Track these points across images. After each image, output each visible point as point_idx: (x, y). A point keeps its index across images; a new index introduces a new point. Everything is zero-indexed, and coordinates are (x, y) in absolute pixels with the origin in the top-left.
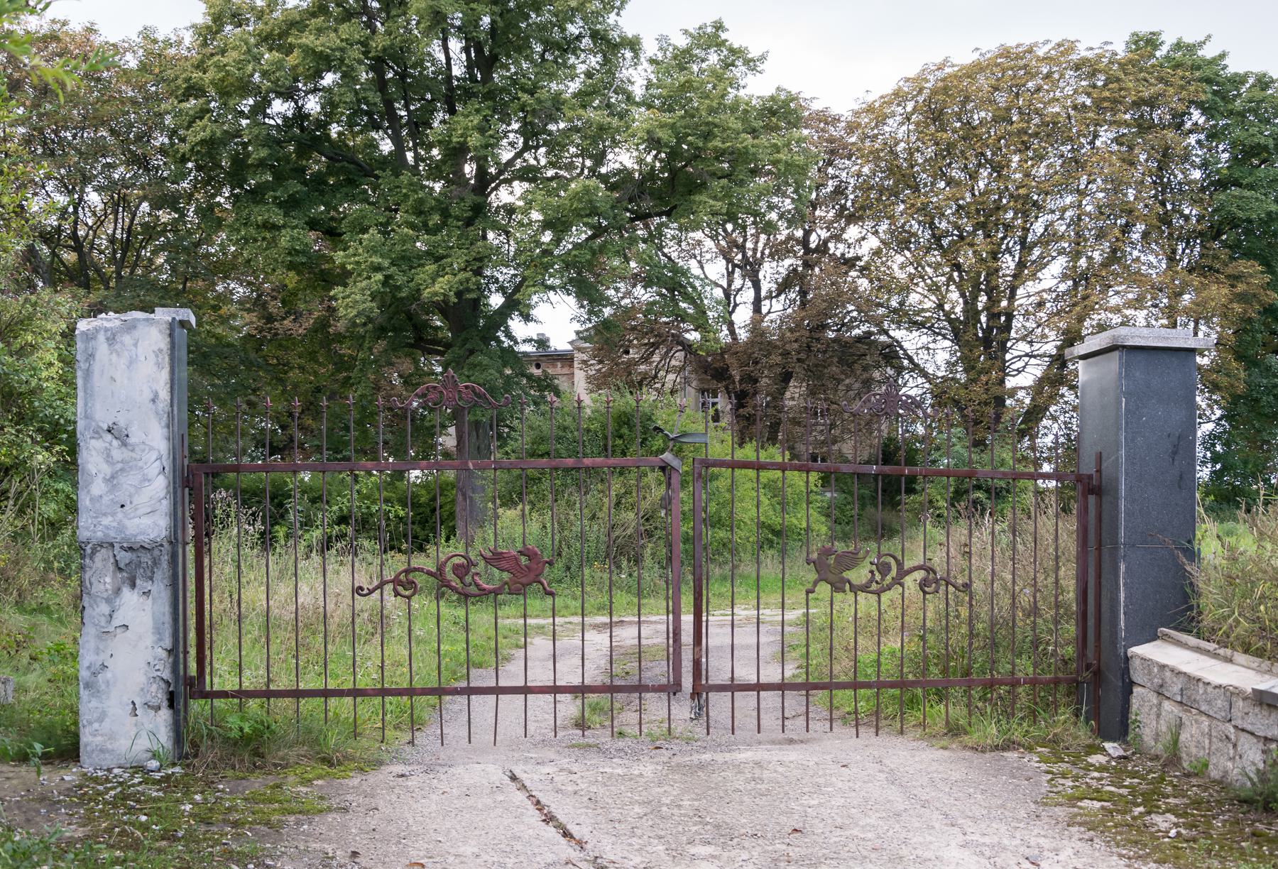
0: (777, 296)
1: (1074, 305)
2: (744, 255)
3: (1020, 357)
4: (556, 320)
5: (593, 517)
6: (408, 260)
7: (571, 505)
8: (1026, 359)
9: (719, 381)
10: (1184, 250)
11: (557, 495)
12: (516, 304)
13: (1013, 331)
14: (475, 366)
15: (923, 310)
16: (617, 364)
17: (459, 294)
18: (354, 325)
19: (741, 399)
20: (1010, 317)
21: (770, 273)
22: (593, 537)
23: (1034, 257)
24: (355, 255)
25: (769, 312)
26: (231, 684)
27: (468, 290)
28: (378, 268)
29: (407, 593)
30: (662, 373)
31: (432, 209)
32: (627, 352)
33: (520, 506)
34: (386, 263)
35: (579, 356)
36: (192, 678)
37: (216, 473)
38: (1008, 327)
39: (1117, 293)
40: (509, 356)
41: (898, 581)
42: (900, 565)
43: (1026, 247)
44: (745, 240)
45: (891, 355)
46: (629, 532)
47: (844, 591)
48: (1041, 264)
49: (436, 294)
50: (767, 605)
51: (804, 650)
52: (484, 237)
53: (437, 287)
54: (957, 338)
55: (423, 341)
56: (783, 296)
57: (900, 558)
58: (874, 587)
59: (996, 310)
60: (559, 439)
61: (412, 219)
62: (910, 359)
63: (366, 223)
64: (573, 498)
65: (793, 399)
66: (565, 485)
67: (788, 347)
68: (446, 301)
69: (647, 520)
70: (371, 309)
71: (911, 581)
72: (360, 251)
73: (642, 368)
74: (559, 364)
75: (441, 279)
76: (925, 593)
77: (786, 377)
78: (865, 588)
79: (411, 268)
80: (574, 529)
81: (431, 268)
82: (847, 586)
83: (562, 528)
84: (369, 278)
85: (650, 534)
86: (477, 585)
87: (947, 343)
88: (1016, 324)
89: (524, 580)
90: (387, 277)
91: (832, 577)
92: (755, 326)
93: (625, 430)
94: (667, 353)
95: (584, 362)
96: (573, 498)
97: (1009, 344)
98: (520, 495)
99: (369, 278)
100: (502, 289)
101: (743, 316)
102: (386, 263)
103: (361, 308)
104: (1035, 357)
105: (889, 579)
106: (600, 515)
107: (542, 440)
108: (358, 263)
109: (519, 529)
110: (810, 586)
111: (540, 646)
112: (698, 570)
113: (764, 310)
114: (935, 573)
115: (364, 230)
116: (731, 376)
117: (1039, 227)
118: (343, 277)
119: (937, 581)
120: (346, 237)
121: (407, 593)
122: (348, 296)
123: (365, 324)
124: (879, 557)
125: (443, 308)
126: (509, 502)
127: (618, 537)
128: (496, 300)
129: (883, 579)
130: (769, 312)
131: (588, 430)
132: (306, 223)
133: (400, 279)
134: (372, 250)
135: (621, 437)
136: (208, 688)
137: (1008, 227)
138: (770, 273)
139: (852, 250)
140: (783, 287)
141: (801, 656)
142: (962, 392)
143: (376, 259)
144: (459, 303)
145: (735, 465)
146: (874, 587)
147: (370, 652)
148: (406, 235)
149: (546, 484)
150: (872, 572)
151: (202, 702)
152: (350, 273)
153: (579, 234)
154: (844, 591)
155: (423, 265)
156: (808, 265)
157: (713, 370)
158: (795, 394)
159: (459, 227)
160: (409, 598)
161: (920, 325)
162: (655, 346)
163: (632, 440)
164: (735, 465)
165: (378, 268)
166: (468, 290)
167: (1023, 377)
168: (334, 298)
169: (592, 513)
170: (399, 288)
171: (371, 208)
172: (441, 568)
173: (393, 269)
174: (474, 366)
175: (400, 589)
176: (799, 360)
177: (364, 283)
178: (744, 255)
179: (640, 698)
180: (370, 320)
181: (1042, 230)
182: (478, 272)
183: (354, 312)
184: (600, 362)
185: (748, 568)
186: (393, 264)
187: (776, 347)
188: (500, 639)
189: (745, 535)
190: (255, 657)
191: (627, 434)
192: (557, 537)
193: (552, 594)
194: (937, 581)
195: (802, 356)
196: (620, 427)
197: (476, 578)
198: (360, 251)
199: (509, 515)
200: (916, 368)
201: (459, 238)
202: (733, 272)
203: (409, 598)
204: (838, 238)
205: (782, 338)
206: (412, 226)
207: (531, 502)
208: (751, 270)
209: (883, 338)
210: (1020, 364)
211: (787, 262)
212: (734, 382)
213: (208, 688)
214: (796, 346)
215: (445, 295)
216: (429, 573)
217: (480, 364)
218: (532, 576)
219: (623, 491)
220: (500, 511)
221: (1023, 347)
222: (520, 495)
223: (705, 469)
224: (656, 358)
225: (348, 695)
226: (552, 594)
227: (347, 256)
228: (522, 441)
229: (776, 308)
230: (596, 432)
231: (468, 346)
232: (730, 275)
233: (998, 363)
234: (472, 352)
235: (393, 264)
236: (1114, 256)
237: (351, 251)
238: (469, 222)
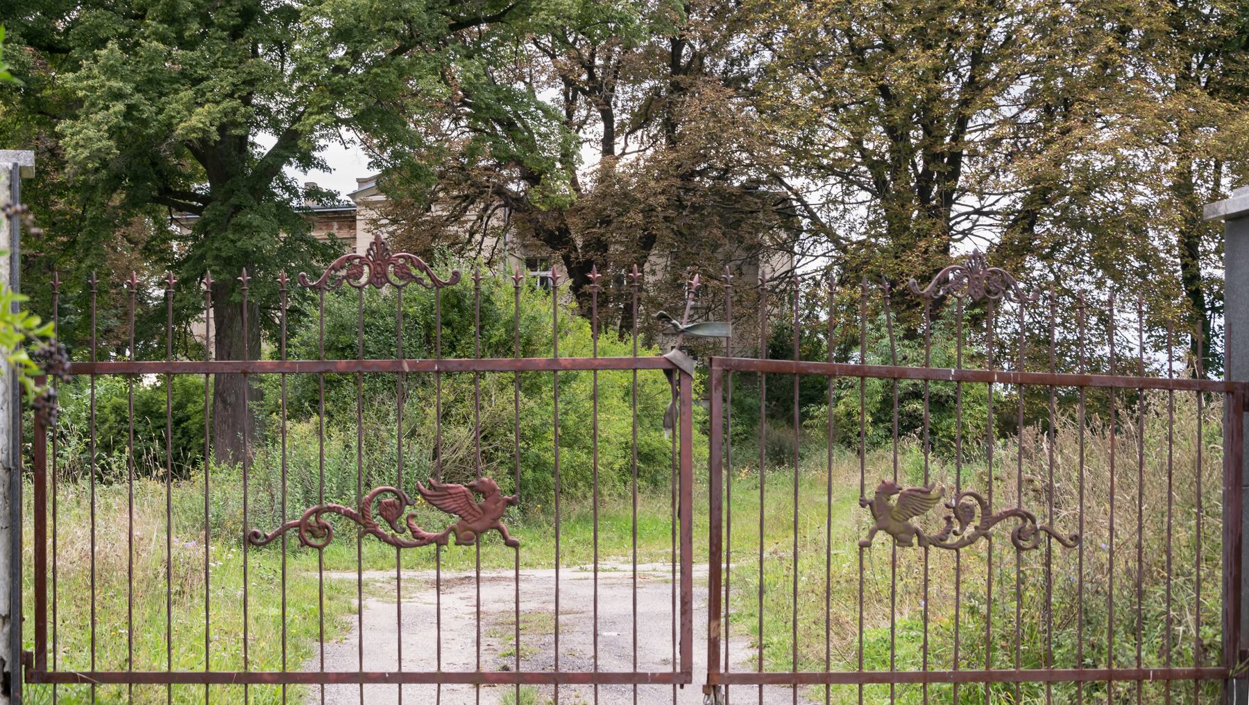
0: (632, 131)
1: (1048, 143)
2: (592, 76)
3: (969, 214)
4: (344, 164)
5: (413, 434)
6: (154, 85)
7: (383, 418)
8: (974, 217)
9: (554, 248)
10: (1200, 66)
11: (364, 401)
12: (295, 146)
13: (961, 178)
14: (243, 227)
15: (835, 149)
16: (417, 225)
17: (222, 129)
18: (85, 171)
19: (579, 273)
20: (955, 159)
21: (626, 97)
22: (412, 460)
23: (990, 76)
24: (88, 78)
25: (623, 154)
26: (79, 663)
27: (236, 125)
28: (118, 96)
29: (319, 542)
30: (478, 237)
31: (188, 14)
32: (429, 209)
33: (315, 418)
34: (128, 88)
35: (364, 215)
36: (29, 655)
37: (1081, 387)
38: (955, 174)
39: (1108, 125)
40: (284, 214)
41: (983, 532)
42: (986, 508)
43: (978, 60)
44: (592, 55)
45: (786, 212)
46: (460, 454)
47: (911, 545)
48: (1000, 85)
49: (193, 129)
50: (653, 558)
51: (756, 621)
52: (255, 53)
53: (194, 121)
54: (880, 189)
55: (171, 195)
56: (639, 133)
57: (985, 497)
58: (952, 539)
59: (938, 149)
60: (367, 328)
61: (162, 28)
62: (813, 216)
63: (102, 34)
64: (384, 408)
65: (653, 272)
66: (375, 390)
67: (651, 201)
68: (204, 141)
69: (485, 438)
70: (109, 148)
71: (1003, 531)
72: (96, 71)
73: (453, 229)
74: (336, 226)
75: (199, 110)
76: (1020, 549)
77: (648, 242)
78: (939, 542)
79: (161, 94)
80: (388, 449)
81: (187, 94)
82: (915, 540)
83: (370, 446)
84: (107, 108)
85: (488, 458)
86: (414, 532)
87: (864, 196)
88: (965, 168)
89: (477, 525)
90: (130, 108)
91: (894, 526)
92: (605, 175)
93: (454, 316)
94: (485, 209)
95: (374, 222)
96: (384, 408)
97: (955, 196)
98: (315, 403)
99: (107, 108)
100: (274, 125)
101: (590, 158)
102: (128, 88)
103: (95, 146)
104: (987, 214)
105: (970, 530)
106: (421, 430)
107: (342, 328)
108: (92, 89)
109: (314, 448)
110: (864, 536)
111: (379, 611)
112: (716, 513)
113: (618, 150)
114: (1034, 521)
115: (102, 43)
116: (579, 246)
117: (998, 34)
118: (70, 106)
119: (1036, 532)
120: (75, 54)
121: (319, 542)
122: (80, 132)
123: (97, 170)
124: (959, 496)
125: (202, 150)
126: (298, 413)
127: (446, 461)
128: (265, 141)
129: (963, 529)
130: (623, 154)
131: (406, 315)
132: (23, 35)
133: (148, 110)
134: (111, 71)
135: (448, 324)
136: (50, 669)
137: (955, 34)
138: (626, 97)
139: (736, 69)
140: (641, 120)
141: (753, 631)
142: (891, 263)
143: (116, 84)
144: (221, 142)
145: (593, 367)
146: (952, 539)
147: (188, 618)
148: (156, 51)
149: (348, 389)
150: (948, 519)
151: (39, 687)
152: (80, 102)
153: (379, 50)
154: (911, 545)
155: (176, 91)
156: (676, 88)
157: (549, 234)
158: (657, 266)
159: (223, 39)
160: (320, 548)
161: (826, 171)
162: (469, 199)
163: (463, 330)
164: (593, 367)
165: (118, 96)
166: (236, 125)
167: (976, 239)
168: (60, 136)
169: (407, 434)
170: (145, 123)
171: (109, 14)
172: (363, 509)
173: (137, 96)
174: (240, 228)
175: (307, 535)
176: (666, 219)
177: (100, 116)
178: (592, 76)
179: (635, 691)
180: (105, 164)
181: (1002, 37)
182: (246, 101)
183: (86, 153)
184: (394, 222)
185: (616, 507)
186: (137, 89)
187: (635, 200)
188: (325, 601)
189: (612, 457)
190: (110, 626)
191: (458, 323)
192: (365, 461)
193: (515, 545)
194: (1036, 532)
195: (671, 213)
196: (447, 312)
197: (413, 522)
198: (96, 71)
199: (301, 430)
200: (820, 229)
201: (224, 53)
202: (575, 98)
203: (320, 548)
204: (716, 50)
205: (643, 186)
206: (163, 39)
207: (329, 414)
208: (600, 94)
209: (777, 189)
210: (966, 225)
211: (647, 85)
212: (576, 250)
213: (50, 669)
214: (662, 199)
215: (204, 131)
216: (349, 515)
217: (249, 225)
218: (487, 520)
219: (452, 398)
220: (288, 424)
221: (971, 200)
222: (315, 403)
223: (563, 374)
224: (472, 215)
225: (237, 682)
226: (515, 545)
227: (79, 79)
228: (312, 330)
229: (634, 151)
230: (414, 317)
231: (233, 200)
232: (570, 105)
233: (941, 223)
234: (238, 209)
235: (137, 89)
236: (1105, 73)
237: (83, 72)
238: (236, 33)
